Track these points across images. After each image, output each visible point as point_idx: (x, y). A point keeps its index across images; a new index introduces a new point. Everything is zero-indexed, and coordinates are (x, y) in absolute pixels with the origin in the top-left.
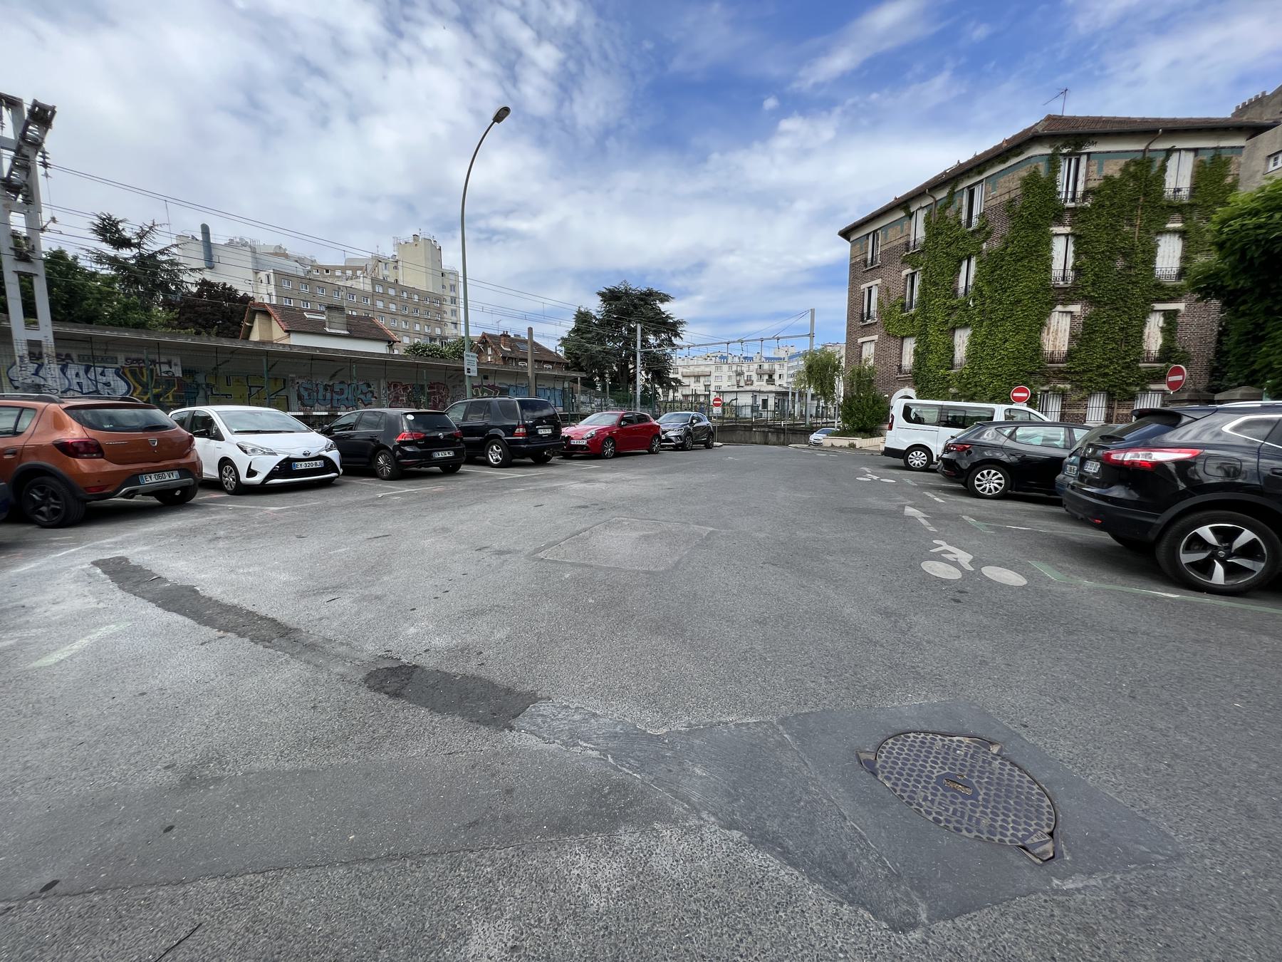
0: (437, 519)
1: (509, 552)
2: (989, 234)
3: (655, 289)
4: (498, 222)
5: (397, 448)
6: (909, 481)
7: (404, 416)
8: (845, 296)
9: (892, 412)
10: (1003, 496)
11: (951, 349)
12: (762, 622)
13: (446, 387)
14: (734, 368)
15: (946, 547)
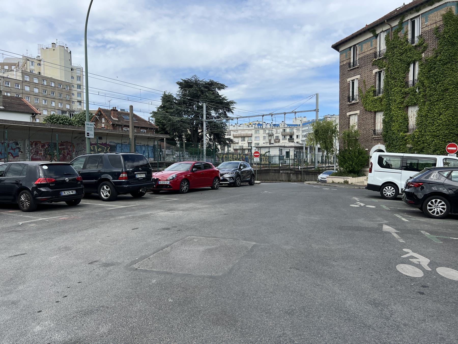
0: (61, 241)
1: (112, 264)
2: (425, 48)
3: (215, 81)
4: (110, 36)
5: (35, 189)
6: (384, 207)
7: (41, 167)
8: (338, 85)
9: (372, 160)
10: (446, 217)
11: (406, 119)
12: (291, 313)
13: (72, 145)
14: (267, 132)
15: (411, 253)
